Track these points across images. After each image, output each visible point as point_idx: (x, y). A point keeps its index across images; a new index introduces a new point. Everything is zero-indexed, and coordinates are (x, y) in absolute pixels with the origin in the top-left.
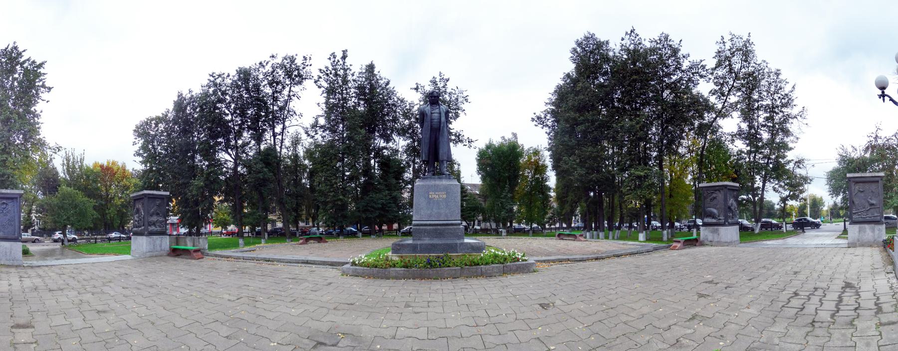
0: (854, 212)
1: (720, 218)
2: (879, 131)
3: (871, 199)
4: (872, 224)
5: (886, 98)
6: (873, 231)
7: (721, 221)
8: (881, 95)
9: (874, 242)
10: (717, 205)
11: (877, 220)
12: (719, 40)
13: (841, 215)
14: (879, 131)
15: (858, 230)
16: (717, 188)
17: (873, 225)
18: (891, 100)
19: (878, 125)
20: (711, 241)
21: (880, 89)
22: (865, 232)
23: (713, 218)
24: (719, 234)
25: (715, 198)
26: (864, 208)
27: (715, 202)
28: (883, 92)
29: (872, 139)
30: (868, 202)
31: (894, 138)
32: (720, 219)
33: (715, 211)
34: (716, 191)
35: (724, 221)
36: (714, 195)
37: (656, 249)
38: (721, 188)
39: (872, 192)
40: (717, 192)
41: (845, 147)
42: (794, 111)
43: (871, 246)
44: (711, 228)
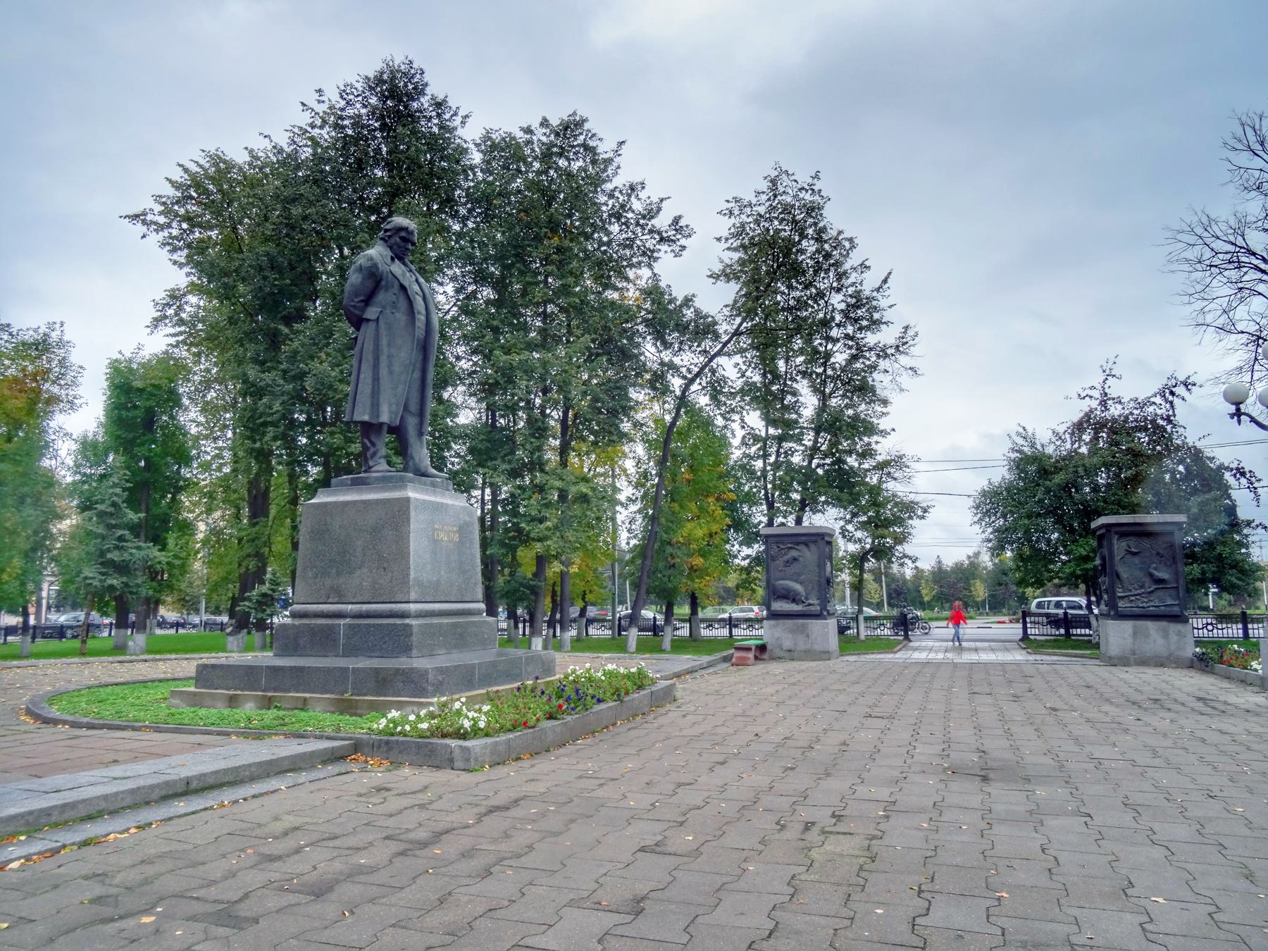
0: (1119, 594)
1: (811, 602)
2: (1111, 381)
3: (1155, 569)
4: (1161, 620)
5: (1243, 417)
6: (1166, 635)
7: (812, 608)
8: (1234, 414)
9: (1168, 658)
10: (799, 575)
11: (1174, 613)
12: (867, 263)
13: (926, 599)
14: (1111, 381)
15: (1130, 631)
16: (804, 538)
17: (1164, 624)
18: (1253, 420)
19: (1106, 367)
20: (790, 651)
21: (1232, 404)
22: (1147, 636)
23: (794, 601)
24: (808, 636)
25: (795, 559)
26: (1142, 587)
27: (794, 568)
28: (1238, 410)
29: (1094, 404)
30: (1151, 575)
31: (1158, 400)
32: (810, 605)
33: (798, 587)
34: (798, 544)
35: (819, 608)
36: (794, 553)
37: (710, 665)
38: (814, 538)
39: (1158, 554)
40: (801, 547)
41: (1030, 431)
42: (885, 336)
43: (1162, 665)
44: (790, 622)
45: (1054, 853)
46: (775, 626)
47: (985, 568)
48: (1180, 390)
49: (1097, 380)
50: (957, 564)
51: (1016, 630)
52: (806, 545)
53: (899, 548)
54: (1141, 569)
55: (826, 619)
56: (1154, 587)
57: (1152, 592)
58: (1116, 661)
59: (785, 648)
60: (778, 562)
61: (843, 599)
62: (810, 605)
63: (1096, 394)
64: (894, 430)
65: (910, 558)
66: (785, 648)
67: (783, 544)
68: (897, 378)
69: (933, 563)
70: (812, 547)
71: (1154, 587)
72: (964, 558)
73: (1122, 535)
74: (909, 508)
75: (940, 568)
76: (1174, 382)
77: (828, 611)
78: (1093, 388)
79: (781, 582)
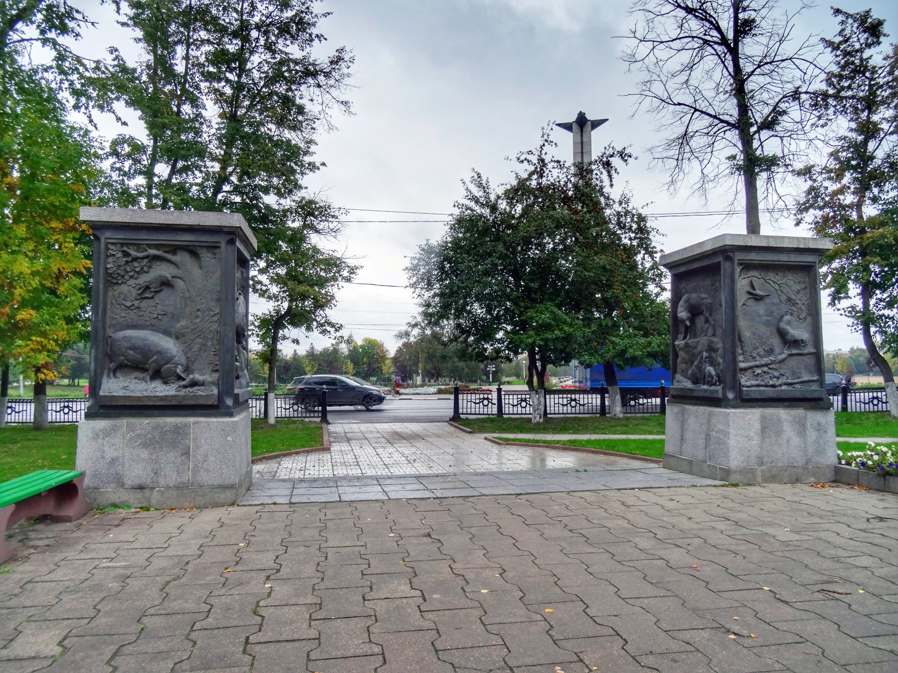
0: (742, 365)
1: (198, 377)
3: (789, 323)
6: (802, 431)
7: (200, 391)
15: (757, 425)
17: (800, 412)
20: (141, 488)
23: (157, 375)
24: (187, 453)
25: (166, 284)
27: (166, 301)
32: (194, 384)
33: (169, 345)
34: (174, 249)
40: (181, 257)
44: (144, 423)
45: (356, 529)
46: (107, 433)
47: (343, 353)
48: (616, 162)
49: (535, 145)
50: (324, 350)
51: (445, 406)
52: (193, 252)
53: (320, 312)
54: (767, 324)
55: (231, 415)
56: (787, 352)
57: (783, 361)
58: (734, 478)
59: (128, 482)
60: (124, 288)
61: (717, 391)
62: (194, 384)
63: (534, 159)
64: (324, 164)
65: (333, 326)
66: (128, 482)
67: (138, 247)
68: (327, 110)
69: (308, 348)
70: (205, 255)
71: (787, 352)
72: (330, 345)
73: (747, 267)
74: (333, 264)
75: (312, 352)
76: (611, 151)
77: (236, 397)
78: (530, 152)
79: (129, 333)
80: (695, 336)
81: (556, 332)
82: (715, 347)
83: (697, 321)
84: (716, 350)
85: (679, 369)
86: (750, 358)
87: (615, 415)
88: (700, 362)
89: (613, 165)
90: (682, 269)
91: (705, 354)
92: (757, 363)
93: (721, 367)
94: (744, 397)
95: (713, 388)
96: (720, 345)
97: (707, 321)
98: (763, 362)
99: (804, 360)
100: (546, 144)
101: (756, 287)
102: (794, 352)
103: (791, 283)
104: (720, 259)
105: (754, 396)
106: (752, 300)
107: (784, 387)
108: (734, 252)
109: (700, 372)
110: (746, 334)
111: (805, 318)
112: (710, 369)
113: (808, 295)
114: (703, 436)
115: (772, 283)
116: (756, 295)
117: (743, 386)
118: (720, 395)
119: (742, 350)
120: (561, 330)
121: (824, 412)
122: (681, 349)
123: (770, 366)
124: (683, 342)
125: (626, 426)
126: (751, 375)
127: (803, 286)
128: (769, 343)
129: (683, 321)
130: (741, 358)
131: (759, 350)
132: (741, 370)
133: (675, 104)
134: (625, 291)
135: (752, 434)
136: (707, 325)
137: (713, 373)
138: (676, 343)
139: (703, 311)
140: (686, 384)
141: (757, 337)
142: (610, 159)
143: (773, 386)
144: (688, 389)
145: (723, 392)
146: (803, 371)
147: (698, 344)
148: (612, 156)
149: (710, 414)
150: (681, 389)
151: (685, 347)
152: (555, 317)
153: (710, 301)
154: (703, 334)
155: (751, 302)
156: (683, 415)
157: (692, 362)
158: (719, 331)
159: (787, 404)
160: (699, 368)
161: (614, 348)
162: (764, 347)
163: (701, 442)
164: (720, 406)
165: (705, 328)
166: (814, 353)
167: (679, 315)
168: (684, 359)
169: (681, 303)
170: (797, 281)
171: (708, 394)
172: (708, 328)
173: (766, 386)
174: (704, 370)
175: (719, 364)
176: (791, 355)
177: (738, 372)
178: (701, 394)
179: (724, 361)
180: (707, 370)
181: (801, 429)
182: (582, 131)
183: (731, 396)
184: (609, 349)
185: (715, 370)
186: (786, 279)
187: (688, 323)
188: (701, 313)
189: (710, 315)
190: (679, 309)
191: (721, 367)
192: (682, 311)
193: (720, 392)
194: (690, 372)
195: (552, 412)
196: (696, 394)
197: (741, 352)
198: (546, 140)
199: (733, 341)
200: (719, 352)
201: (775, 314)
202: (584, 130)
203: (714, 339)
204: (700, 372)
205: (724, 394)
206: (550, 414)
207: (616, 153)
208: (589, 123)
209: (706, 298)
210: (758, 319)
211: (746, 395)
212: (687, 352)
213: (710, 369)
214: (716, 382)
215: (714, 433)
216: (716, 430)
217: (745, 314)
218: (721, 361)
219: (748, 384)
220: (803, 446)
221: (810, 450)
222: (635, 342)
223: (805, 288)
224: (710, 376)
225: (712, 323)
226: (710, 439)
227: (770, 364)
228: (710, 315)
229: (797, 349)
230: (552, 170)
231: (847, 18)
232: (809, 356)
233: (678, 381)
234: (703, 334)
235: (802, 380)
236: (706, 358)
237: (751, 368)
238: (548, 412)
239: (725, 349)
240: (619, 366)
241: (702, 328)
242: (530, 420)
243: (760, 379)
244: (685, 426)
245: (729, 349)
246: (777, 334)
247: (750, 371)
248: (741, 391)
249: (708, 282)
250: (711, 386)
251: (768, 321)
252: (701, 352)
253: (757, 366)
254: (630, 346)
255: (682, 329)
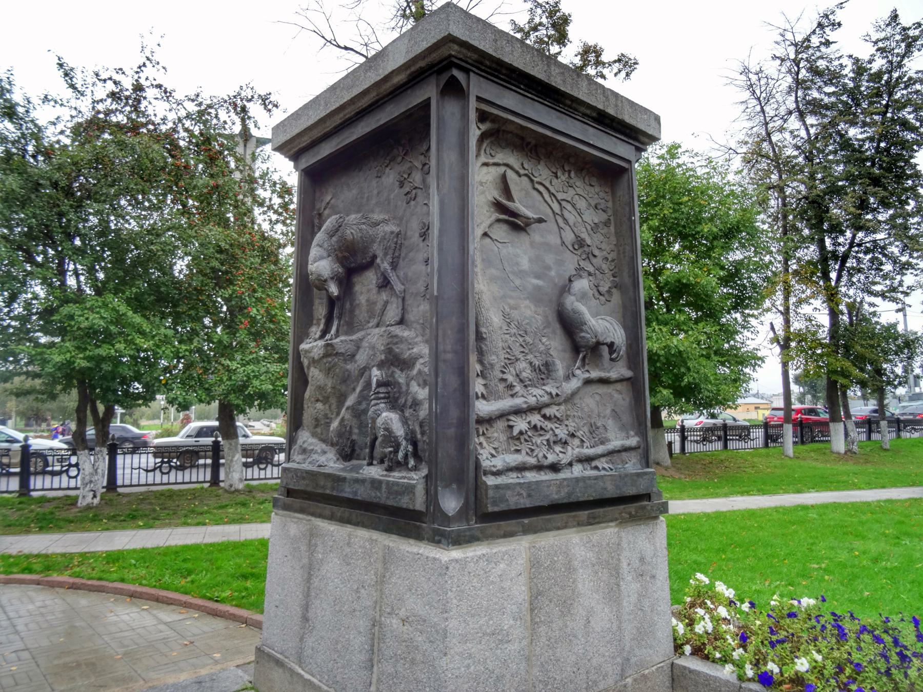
0: (483, 408)
17: (608, 533)
54: (536, 297)
56: (581, 374)
71: (581, 374)
80: (351, 327)
81: (117, 346)
82: (406, 355)
83: (357, 288)
84: (405, 364)
85: (307, 417)
86: (501, 387)
87: (231, 486)
88: (363, 397)
89: (251, 114)
90: (326, 150)
91: (376, 374)
92: (518, 401)
93: (423, 413)
94: (491, 509)
95: (396, 476)
96: (423, 349)
97: (385, 284)
98: (532, 401)
99: (611, 396)
100: (148, 63)
101: (515, 194)
102: (595, 374)
103: (582, 204)
104: (429, 91)
105: (515, 501)
106: (505, 227)
107: (578, 470)
108: (467, 71)
109: (362, 426)
110: (494, 319)
111: (609, 292)
112: (389, 419)
113: (613, 240)
114: (363, 624)
115: (546, 196)
116: (514, 214)
117: (485, 473)
118: (419, 504)
119: (481, 362)
120: (130, 343)
121: (651, 523)
122: (314, 362)
123: (548, 411)
124: (321, 343)
125: (244, 505)
126: (503, 437)
127: (604, 217)
128: (542, 348)
129: (321, 284)
130: (478, 386)
131: (522, 365)
132: (480, 421)
133: (339, 46)
134: (255, 291)
135: (507, 623)
136: (384, 296)
137: (399, 430)
138: (304, 346)
139: (375, 257)
140: (322, 459)
141: (513, 331)
142: (248, 105)
143: (555, 468)
144: (328, 476)
145: (427, 492)
146: (610, 423)
147: (358, 348)
148: (249, 101)
149: (388, 557)
150: (309, 473)
151: (326, 355)
152: (119, 320)
153: (395, 229)
154: (374, 322)
155: (501, 232)
156: (312, 548)
157: (342, 398)
158: (420, 310)
159: (584, 514)
160: (359, 413)
161: (230, 379)
162: (530, 357)
163: (358, 641)
164: (417, 535)
165: (379, 306)
166: (628, 379)
167: (312, 267)
168: (320, 388)
169: (320, 236)
170: (593, 204)
171: (382, 497)
172: (386, 303)
173: (539, 468)
174: (374, 421)
175: (416, 404)
176: (588, 382)
177: (473, 424)
178: (363, 493)
179: (434, 395)
180: (380, 421)
181: (613, 581)
182: (245, 146)
183: (451, 504)
184: (221, 380)
185: (405, 421)
186: (571, 192)
187: (334, 289)
188: (370, 264)
189: (394, 266)
190: (314, 252)
191: (423, 413)
192: (321, 258)
193: (420, 490)
194: (335, 424)
195: (127, 482)
196: (347, 492)
197: (478, 368)
198: (148, 59)
199: (462, 341)
200: (418, 366)
201: (553, 273)
202: (248, 146)
203: (405, 333)
204: (362, 426)
205: (432, 498)
206: (123, 486)
207: (256, 97)
208: (254, 140)
209: (385, 221)
210: (518, 282)
211: (495, 503)
212: (328, 371)
213: (389, 419)
214: (406, 456)
215: (395, 622)
216: (403, 613)
217: (487, 262)
218: (422, 393)
219: (498, 463)
220: (615, 628)
221: (629, 630)
222: (263, 369)
223: (607, 224)
224: (391, 438)
225: (398, 287)
226: (382, 639)
227: (547, 405)
228: (394, 266)
229: (601, 370)
230: (153, 101)
231: (536, 7)
232: (619, 386)
233: (304, 451)
234: (374, 322)
235: (611, 446)
236: (380, 384)
237: (503, 415)
238: (119, 482)
239: (436, 355)
240: (238, 406)
241: (371, 304)
242: (72, 502)
243: (525, 447)
244: (316, 582)
245: (449, 356)
246: (557, 326)
247: (501, 424)
248: (478, 488)
249: (390, 178)
250: (390, 469)
251: (538, 288)
252: (365, 370)
253: (518, 412)
254: (255, 376)
255: (320, 311)
